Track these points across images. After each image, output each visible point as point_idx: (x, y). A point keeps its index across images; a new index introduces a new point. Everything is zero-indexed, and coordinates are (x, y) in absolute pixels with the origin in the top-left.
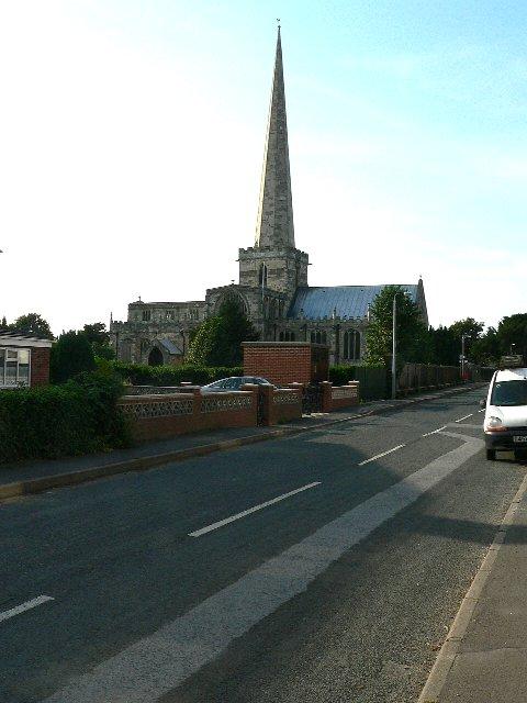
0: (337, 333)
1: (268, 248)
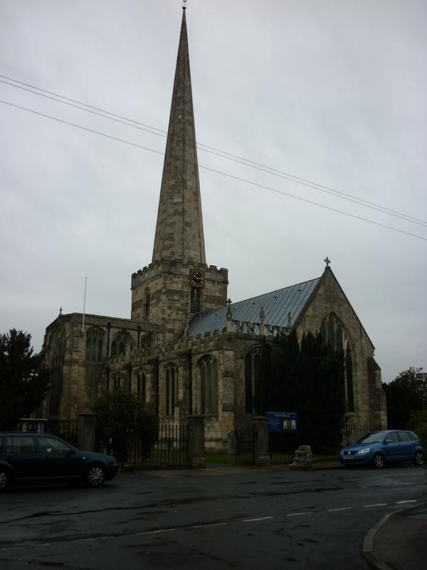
0: (155, 372)
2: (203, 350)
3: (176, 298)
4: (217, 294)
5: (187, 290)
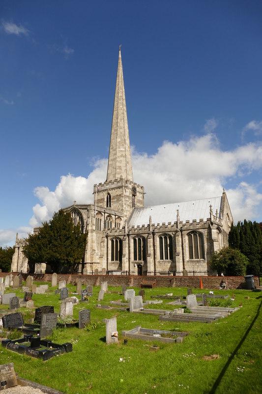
1: (110, 182)
2: (192, 228)
3: (127, 199)
4: (141, 199)
5: (131, 196)
